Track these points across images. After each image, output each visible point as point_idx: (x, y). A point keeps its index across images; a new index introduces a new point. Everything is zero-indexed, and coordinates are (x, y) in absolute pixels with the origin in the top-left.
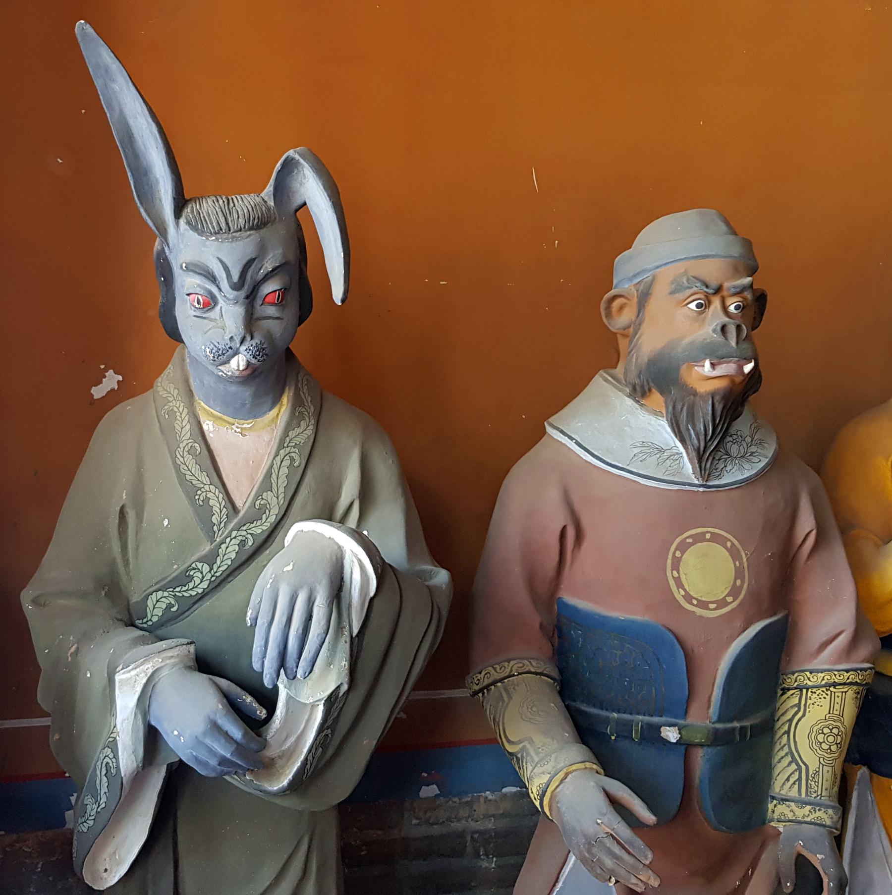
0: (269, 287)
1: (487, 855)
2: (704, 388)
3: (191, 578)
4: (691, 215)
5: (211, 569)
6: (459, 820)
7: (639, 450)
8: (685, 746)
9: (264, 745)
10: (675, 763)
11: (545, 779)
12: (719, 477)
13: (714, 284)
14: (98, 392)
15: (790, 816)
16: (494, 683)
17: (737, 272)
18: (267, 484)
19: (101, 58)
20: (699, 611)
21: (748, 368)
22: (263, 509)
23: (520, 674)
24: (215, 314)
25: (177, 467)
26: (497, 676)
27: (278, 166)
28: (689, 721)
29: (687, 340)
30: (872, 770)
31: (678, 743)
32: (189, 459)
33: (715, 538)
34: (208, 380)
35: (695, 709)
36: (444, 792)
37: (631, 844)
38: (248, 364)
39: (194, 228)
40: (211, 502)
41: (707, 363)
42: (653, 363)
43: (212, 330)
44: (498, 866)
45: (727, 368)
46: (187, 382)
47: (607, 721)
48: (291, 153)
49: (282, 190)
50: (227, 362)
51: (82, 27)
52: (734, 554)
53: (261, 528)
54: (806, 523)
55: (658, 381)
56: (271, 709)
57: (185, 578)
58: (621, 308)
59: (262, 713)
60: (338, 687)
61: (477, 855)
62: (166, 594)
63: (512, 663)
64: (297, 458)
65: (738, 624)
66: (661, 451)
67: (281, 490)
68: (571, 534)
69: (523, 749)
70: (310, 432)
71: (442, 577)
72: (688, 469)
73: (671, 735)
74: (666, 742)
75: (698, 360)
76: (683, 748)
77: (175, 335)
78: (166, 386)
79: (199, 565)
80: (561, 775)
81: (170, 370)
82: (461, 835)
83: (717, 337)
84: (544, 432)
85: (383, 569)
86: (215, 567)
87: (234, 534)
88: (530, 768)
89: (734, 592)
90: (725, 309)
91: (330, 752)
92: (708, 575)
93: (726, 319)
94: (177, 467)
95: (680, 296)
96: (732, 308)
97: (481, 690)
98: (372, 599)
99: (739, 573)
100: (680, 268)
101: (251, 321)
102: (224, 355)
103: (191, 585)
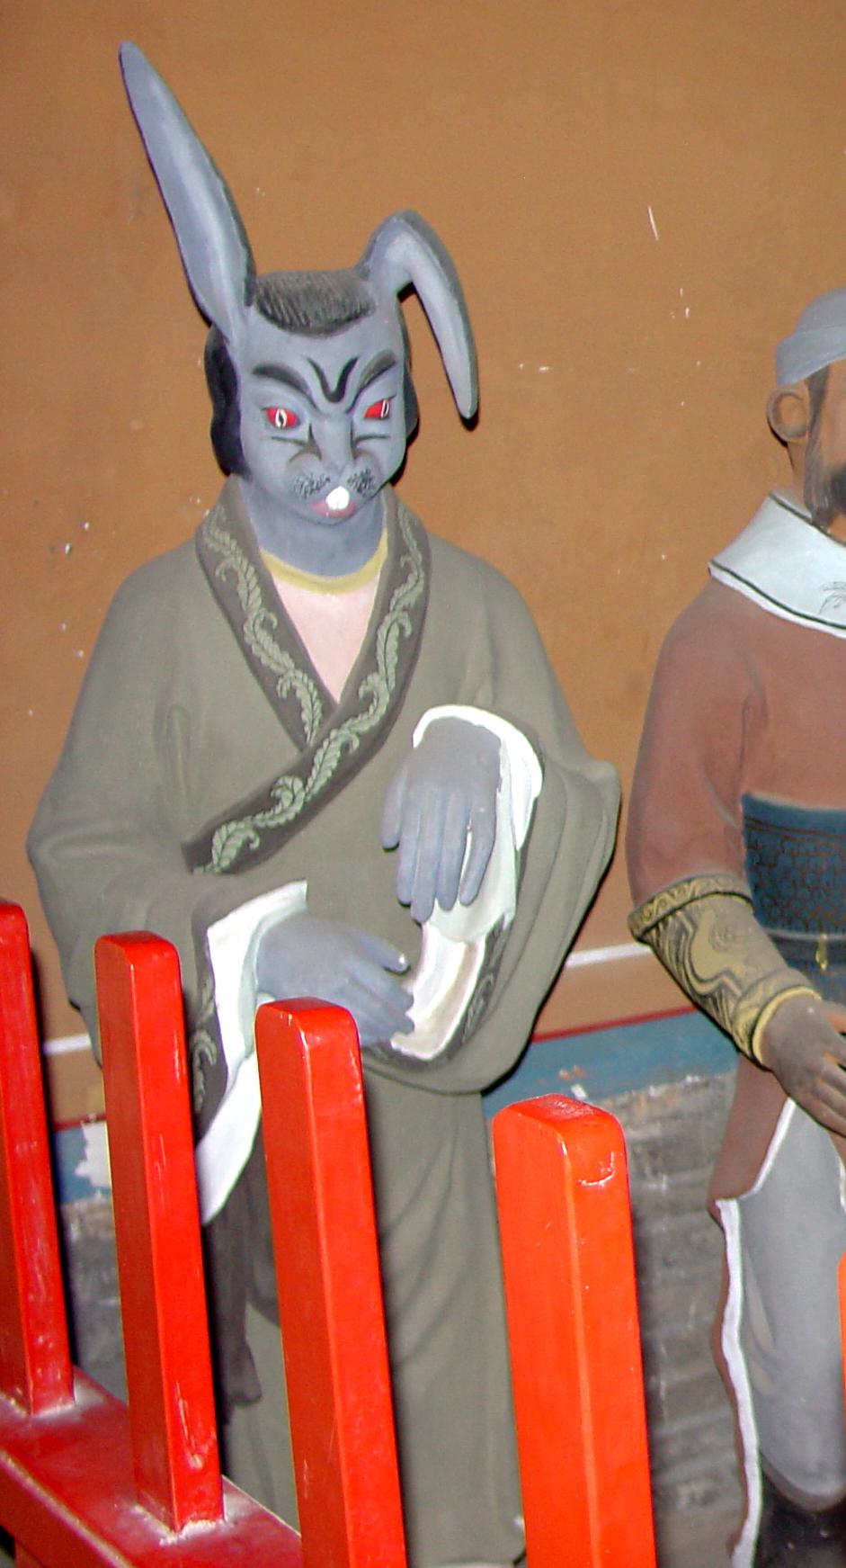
3: (277, 801)
5: (305, 784)
7: (829, 594)
11: (753, 1013)
16: (673, 912)
18: (369, 661)
19: (153, 93)
22: (369, 699)
23: (704, 896)
26: (676, 903)
32: (264, 636)
40: (298, 694)
44: (670, 1186)
53: (367, 723)
57: (265, 801)
60: (503, 918)
61: (642, 1175)
62: (242, 825)
63: (694, 883)
67: (392, 671)
79: (289, 781)
86: (310, 782)
87: (333, 734)
88: (732, 1006)
97: (656, 926)
103: (278, 809)
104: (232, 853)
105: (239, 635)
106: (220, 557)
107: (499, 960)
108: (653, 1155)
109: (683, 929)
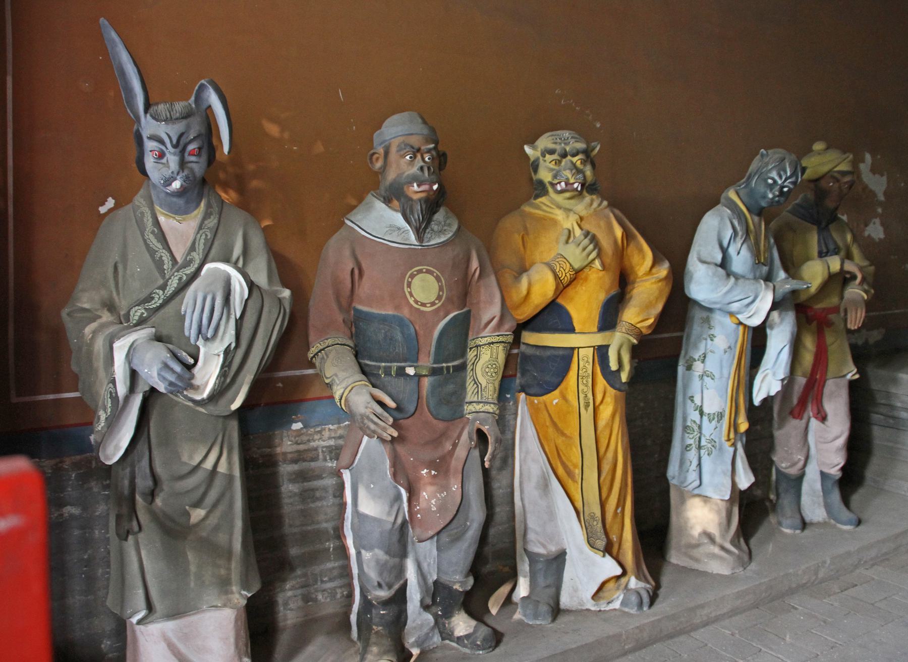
0: (191, 147)
1: (331, 459)
2: (416, 197)
3: (153, 298)
4: (406, 114)
6: (314, 441)
8: (418, 376)
9: (193, 377)
10: (413, 385)
11: (342, 391)
12: (429, 241)
13: (416, 146)
14: (103, 210)
15: (474, 410)
16: (320, 351)
17: (427, 141)
18: (193, 248)
20: (422, 308)
21: (435, 187)
22: (191, 261)
24: (164, 161)
25: (145, 241)
26: (322, 347)
27: (197, 88)
28: (420, 363)
29: (406, 174)
30: (527, 394)
31: (415, 375)
32: (151, 237)
33: (428, 272)
34: (162, 195)
35: (422, 356)
36: (306, 426)
37: (382, 415)
38: (182, 186)
39: (154, 118)
41: (415, 185)
42: (391, 185)
43: (163, 169)
45: (425, 187)
46: (150, 197)
47: (379, 367)
48: (203, 81)
49: (198, 99)
50: (170, 184)
51: (102, 20)
52: (438, 279)
54: (475, 264)
55: (394, 195)
56: (196, 361)
58: (377, 159)
59: (192, 361)
60: (230, 345)
61: (325, 460)
64: (209, 234)
65: (442, 314)
66: (399, 229)
67: (201, 251)
68: (356, 272)
69: (333, 380)
70: (216, 221)
71: (286, 293)
72: (413, 238)
73: (411, 371)
74: (408, 375)
75: (410, 183)
76: (417, 378)
77: (144, 172)
78: (139, 200)
80: (350, 388)
81: (142, 192)
82: (316, 449)
83: (419, 172)
84: (344, 223)
85: (251, 285)
89: (439, 298)
90: (423, 159)
91: (228, 380)
92: (425, 289)
93: (422, 164)
94: (145, 241)
95: (402, 153)
96: (427, 159)
98: (247, 300)
99: (441, 289)
100: (401, 139)
101: (182, 164)
102: (168, 182)
104: (136, 318)
105: (143, 236)
106: (139, 207)
107: (231, 362)
108: (331, 452)
109: (323, 358)
